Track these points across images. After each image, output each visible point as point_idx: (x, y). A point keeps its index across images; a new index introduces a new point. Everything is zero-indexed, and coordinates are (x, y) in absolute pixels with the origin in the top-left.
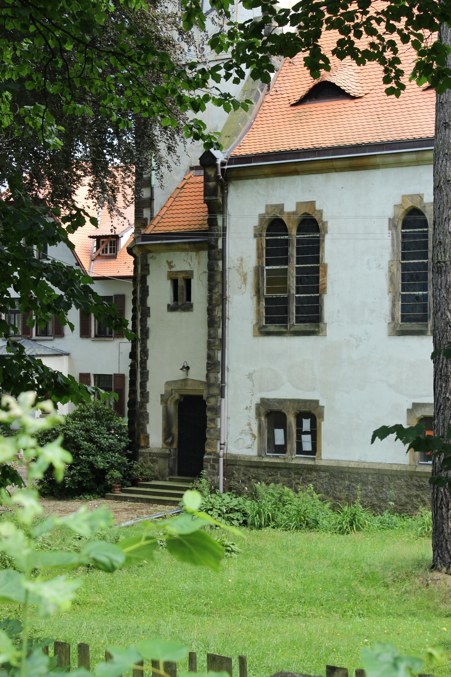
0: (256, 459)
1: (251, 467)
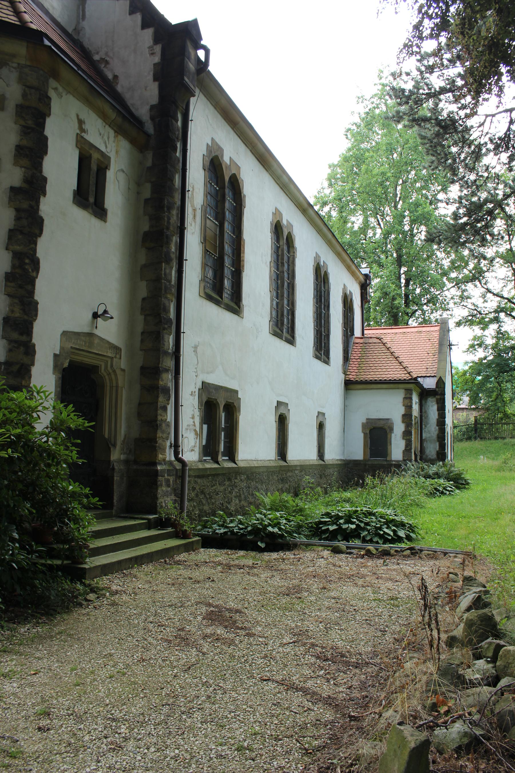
0: (200, 466)
1: (199, 477)
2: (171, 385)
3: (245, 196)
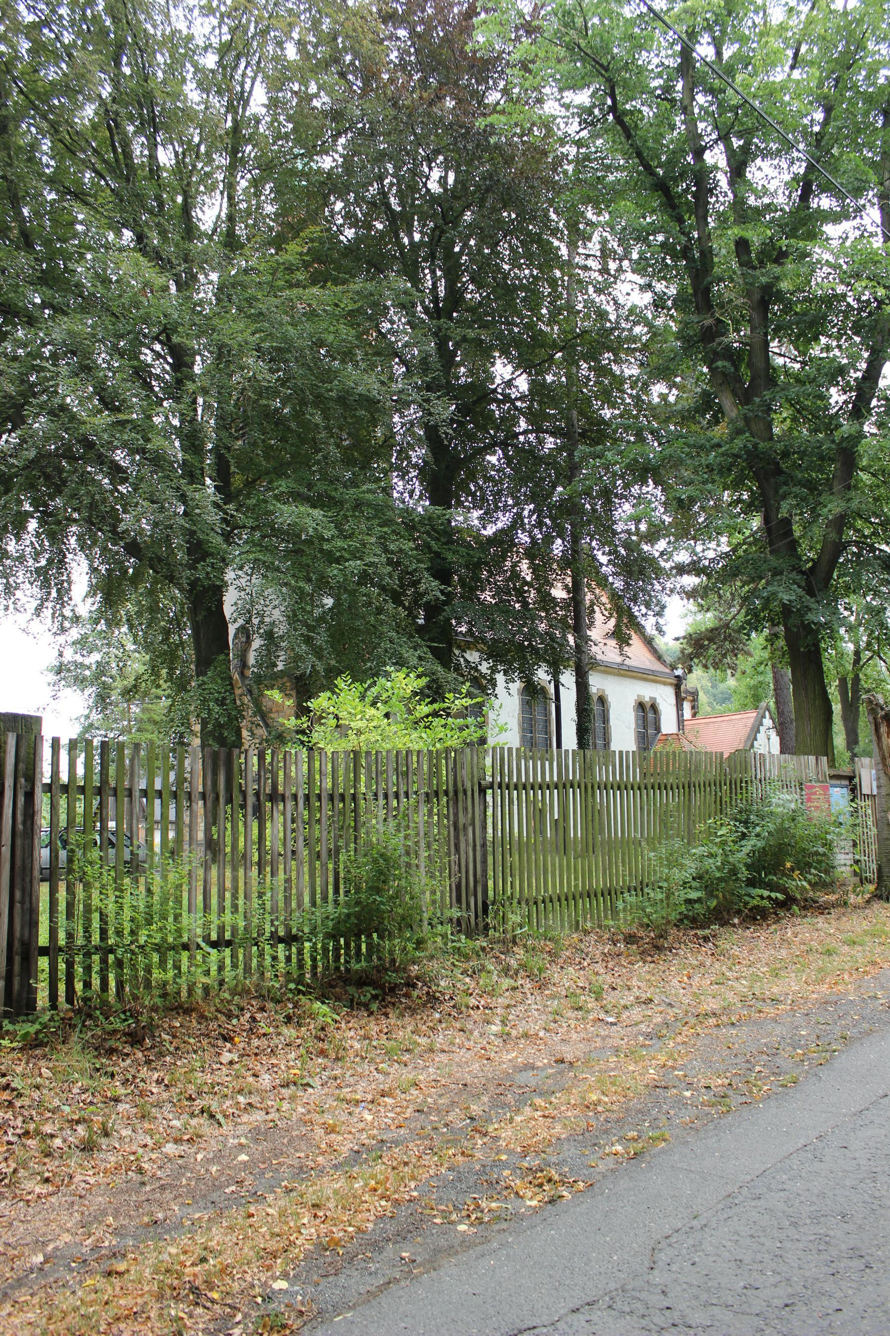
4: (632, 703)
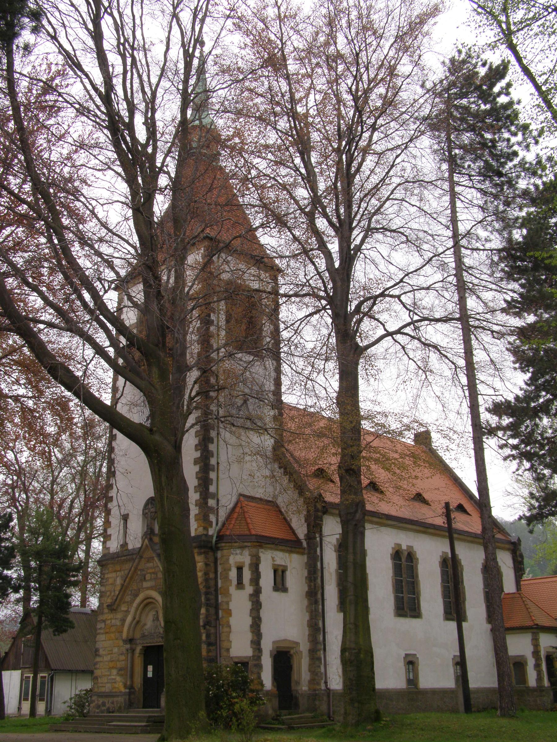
2: (322, 656)
3: (417, 559)
4: (388, 551)
